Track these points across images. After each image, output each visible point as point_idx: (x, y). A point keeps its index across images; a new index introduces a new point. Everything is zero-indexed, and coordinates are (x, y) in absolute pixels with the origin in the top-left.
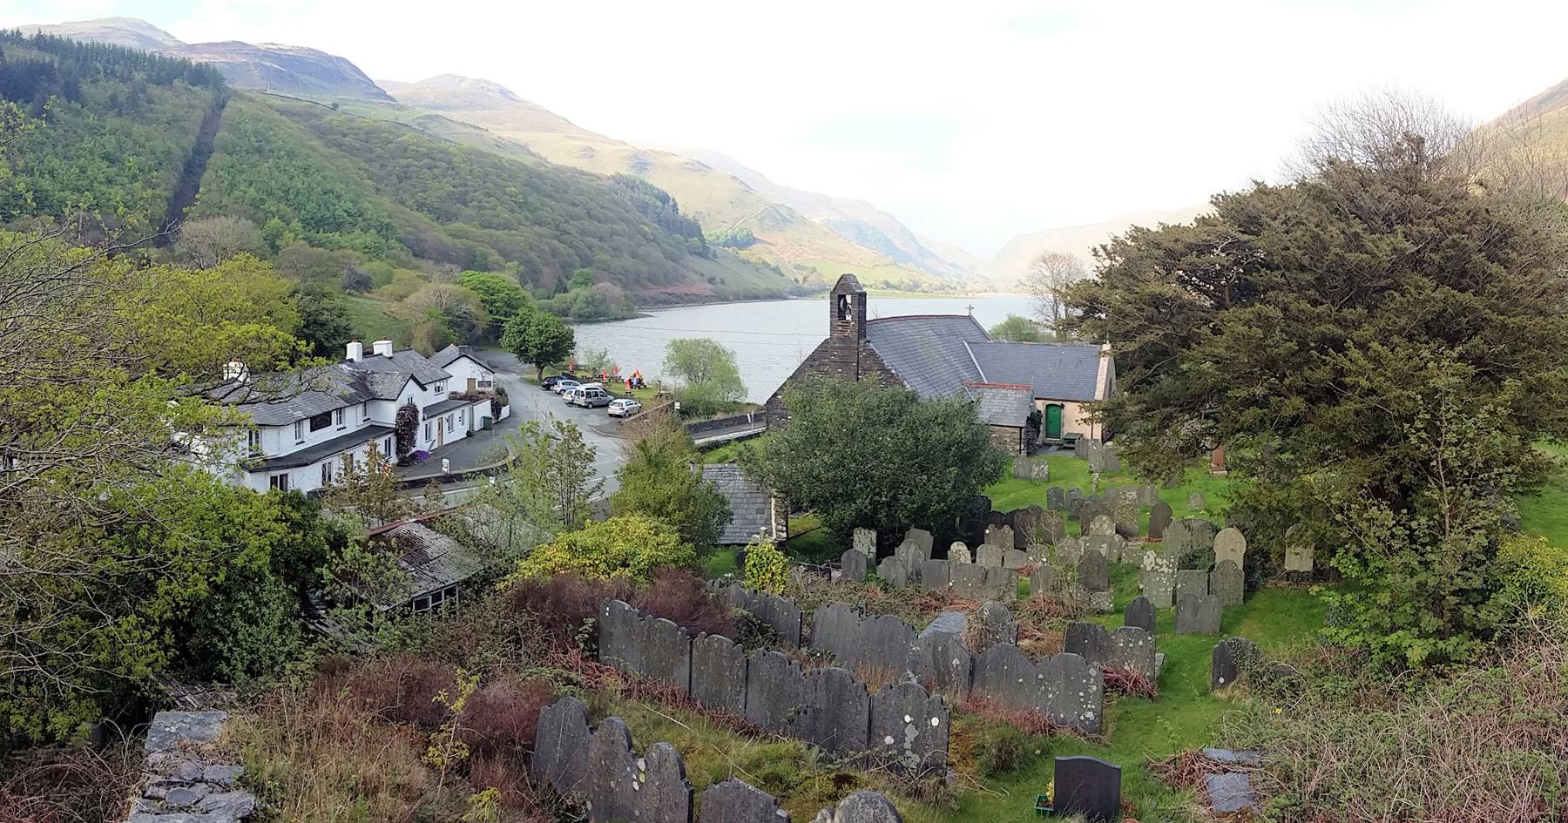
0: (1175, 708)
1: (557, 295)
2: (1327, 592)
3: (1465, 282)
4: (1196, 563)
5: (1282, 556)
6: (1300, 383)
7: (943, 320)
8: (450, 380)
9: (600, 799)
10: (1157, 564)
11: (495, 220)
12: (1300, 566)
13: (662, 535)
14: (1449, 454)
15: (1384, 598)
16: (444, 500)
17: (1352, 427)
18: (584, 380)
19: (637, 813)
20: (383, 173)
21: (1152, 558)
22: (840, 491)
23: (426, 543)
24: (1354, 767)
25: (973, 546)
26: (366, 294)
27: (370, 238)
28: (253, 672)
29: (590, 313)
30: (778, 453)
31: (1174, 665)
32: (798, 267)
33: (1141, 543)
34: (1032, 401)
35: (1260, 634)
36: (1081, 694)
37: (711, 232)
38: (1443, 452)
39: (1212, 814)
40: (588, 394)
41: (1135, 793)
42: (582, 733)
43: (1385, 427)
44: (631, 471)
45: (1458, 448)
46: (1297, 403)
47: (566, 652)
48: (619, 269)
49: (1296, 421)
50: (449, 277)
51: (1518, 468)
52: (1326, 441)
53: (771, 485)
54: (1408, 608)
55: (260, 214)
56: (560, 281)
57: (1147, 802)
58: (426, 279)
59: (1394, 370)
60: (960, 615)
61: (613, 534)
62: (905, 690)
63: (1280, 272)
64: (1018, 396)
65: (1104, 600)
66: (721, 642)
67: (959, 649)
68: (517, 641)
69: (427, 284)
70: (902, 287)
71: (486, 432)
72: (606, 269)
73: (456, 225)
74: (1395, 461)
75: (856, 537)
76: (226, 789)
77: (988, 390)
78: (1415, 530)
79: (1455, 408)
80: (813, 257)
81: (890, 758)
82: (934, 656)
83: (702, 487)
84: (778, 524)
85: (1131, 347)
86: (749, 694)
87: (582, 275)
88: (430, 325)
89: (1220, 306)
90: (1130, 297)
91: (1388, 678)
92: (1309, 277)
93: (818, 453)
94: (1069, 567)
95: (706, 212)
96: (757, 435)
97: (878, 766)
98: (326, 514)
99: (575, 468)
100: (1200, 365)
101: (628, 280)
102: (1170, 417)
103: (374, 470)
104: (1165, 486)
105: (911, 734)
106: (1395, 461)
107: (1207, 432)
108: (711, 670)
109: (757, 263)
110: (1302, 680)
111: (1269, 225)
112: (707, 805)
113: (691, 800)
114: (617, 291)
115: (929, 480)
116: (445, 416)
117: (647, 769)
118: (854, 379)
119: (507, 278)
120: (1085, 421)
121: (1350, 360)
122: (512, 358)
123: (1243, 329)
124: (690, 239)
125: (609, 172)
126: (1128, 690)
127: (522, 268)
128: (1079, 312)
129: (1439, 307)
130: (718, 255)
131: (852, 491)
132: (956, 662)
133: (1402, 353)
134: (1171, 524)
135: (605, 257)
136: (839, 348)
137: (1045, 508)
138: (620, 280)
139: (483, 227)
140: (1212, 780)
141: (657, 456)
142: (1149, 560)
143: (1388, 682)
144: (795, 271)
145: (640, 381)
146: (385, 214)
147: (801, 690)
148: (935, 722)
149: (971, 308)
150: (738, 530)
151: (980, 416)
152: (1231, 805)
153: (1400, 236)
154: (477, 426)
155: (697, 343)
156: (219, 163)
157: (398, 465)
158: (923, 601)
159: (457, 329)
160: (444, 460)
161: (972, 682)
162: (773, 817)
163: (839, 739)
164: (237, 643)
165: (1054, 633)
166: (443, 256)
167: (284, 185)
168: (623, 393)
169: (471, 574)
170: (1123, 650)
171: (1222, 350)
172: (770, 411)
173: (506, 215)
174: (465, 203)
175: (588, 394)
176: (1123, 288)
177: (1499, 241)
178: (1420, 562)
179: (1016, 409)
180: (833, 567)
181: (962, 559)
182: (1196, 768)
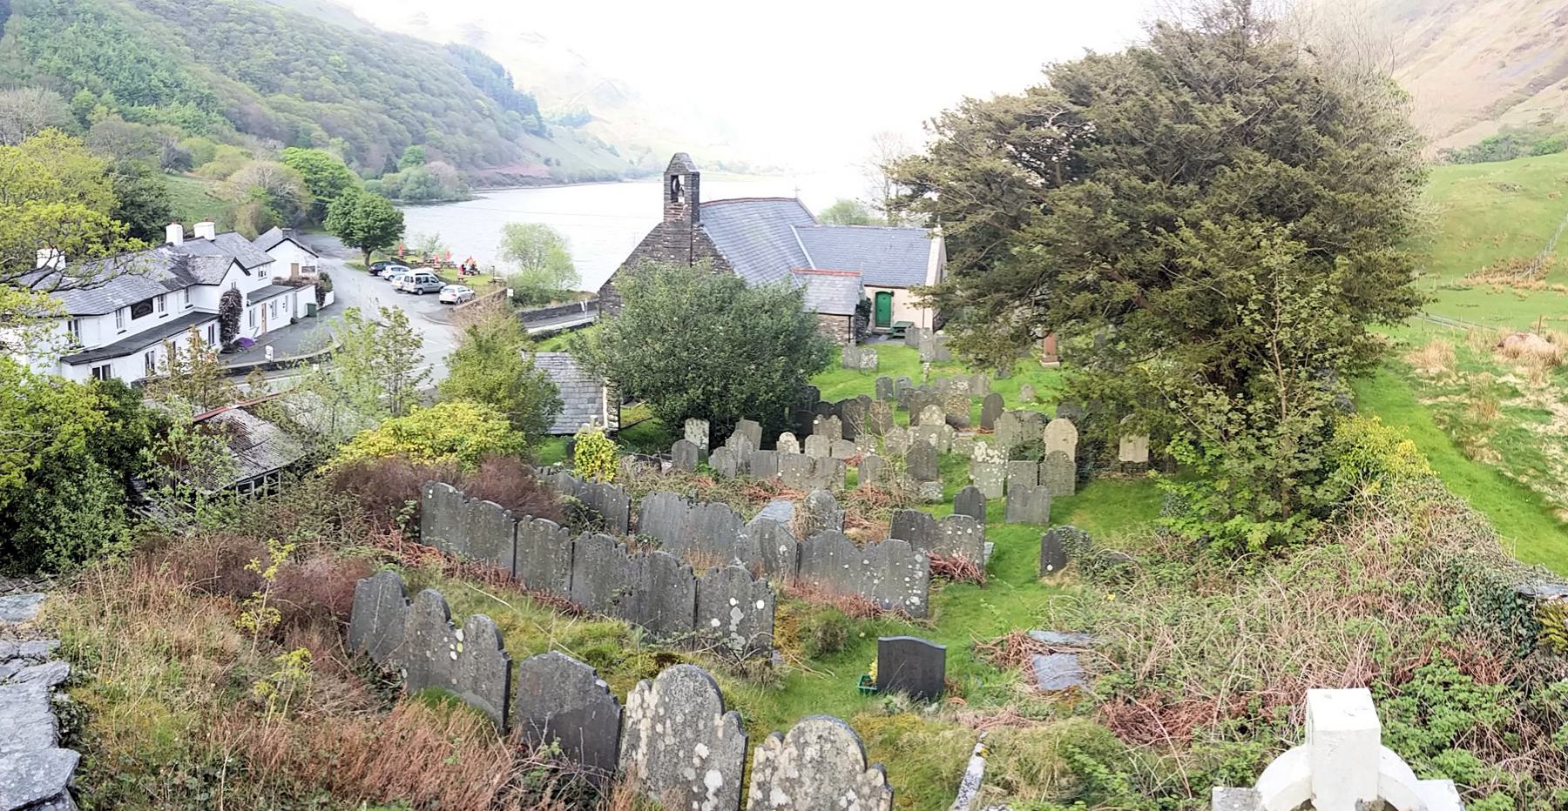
0: (1004, 594)
1: (385, 175)
2: (1162, 481)
3: (1296, 156)
4: (1026, 454)
5: (1117, 447)
6: (1132, 266)
7: (770, 203)
8: (273, 264)
9: (415, 669)
10: (988, 455)
11: (318, 91)
12: (1135, 458)
13: (491, 421)
14: (1284, 335)
15: (1223, 485)
16: (267, 388)
17: (1185, 312)
18: (415, 265)
19: (454, 681)
20: (201, 38)
21: (983, 448)
22: (671, 381)
23: (249, 430)
24: (1190, 647)
25: (801, 436)
26: (186, 173)
27: (190, 111)
28: (78, 558)
29: (422, 194)
30: (610, 340)
31: (1004, 553)
32: (633, 148)
33: (973, 434)
34: (861, 288)
35: (1092, 524)
37: (549, 109)
38: (1277, 333)
39: (1038, 692)
41: (959, 674)
43: (1220, 310)
44: (460, 356)
45: (1292, 329)
46: (1129, 288)
47: (387, 533)
48: (453, 147)
49: (1129, 306)
51: (1351, 349)
52: (1159, 327)
54: (1246, 494)
55: (67, 86)
56: (389, 159)
57: (973, 682)
58: (249, 156)
59: (1227, 250)
60: (789, 503)
61: (440, 420)
62: (730, 574)
63: (1110, 147)
65: (933, 490)
66: (546, 526)
68: (337, 522)
69: (251, 161)
71: (310, 319)
72: (439, 147)
74: (1230, 346)
75: (687, 428)
76: (42, 660)
77: (816, 276)
78: (1251, 414)
79: (1290, 288)
81: (717, 640)
82: (761, 543)
83: (534, 375)
85: (961, 228)
87: (412, 153)
88: (253, 206)
89: (1052, 184)
90: (960, 174)
91: (1227, 563)
92: (1139, 150)
93: (650, 341)
94: (897, 457)
97: (704, 647)
98: (149, 403)
99: (401, 355)
100: (1030, 251)
101: (464, 160)
102: (1001, 303)
103: (196, 357)
104: (1000, 375)
105: (737, 616)
106: (1230, 346)
107: (1038, 320)
110: (1136, 567)
111: (1098, 95)
112: (524, 676)
113: (509, 671)
114: (451, 171)
115: (757, 369)
116: (269, 302)
118: (687, 264)
119: (331, 155)
120: (915, 305)
121: (1182, 240)
122: (335, 242)
123: (1072, 208)
124: (527, 117)
125: (444, 40)
126: (956, 576)
127: (347, 144)
128: (907, 191)
129: (1271, 182)
131: (684, 381)
132: (783, 548)
133: (1233, 231)
135: (439, 134)
136: (672, 233)
137: (874, 398)
138: (454, 159)
139: (306, 99)
140: (1038, 660)
141: (487, 341)
142: (980, 451)
143: (1228, 566)
145: (473, 267)
146: (206, 84)
147: (627, 572)
148: (760, 604)
150: (569, 420)
152: (1057, 684)
153: (1229, 107)
154: (302, 313)
155: (533, 228)
156: (18, 26)
157: (222, 352)
158: (752, 491)
159: (281, 211)
160: (268, 347)
162: (592, 687)
163: (663, 622)
164: (59, 529)
165: (880, 523)
166: (266, 131)
167: (93, 52)
168: (456, 279)
169: (293, 460)
170: (951, 538)
171: (1052, 231)
172: (604, 298)
173: (330, 86)
174: (287, 73)
175: (418, 279)
176: (953, 164)
177: (1328, 112)
178: (1257, 448)
180: (663, 457)
181: (791, 450)
182: (1022, 649)
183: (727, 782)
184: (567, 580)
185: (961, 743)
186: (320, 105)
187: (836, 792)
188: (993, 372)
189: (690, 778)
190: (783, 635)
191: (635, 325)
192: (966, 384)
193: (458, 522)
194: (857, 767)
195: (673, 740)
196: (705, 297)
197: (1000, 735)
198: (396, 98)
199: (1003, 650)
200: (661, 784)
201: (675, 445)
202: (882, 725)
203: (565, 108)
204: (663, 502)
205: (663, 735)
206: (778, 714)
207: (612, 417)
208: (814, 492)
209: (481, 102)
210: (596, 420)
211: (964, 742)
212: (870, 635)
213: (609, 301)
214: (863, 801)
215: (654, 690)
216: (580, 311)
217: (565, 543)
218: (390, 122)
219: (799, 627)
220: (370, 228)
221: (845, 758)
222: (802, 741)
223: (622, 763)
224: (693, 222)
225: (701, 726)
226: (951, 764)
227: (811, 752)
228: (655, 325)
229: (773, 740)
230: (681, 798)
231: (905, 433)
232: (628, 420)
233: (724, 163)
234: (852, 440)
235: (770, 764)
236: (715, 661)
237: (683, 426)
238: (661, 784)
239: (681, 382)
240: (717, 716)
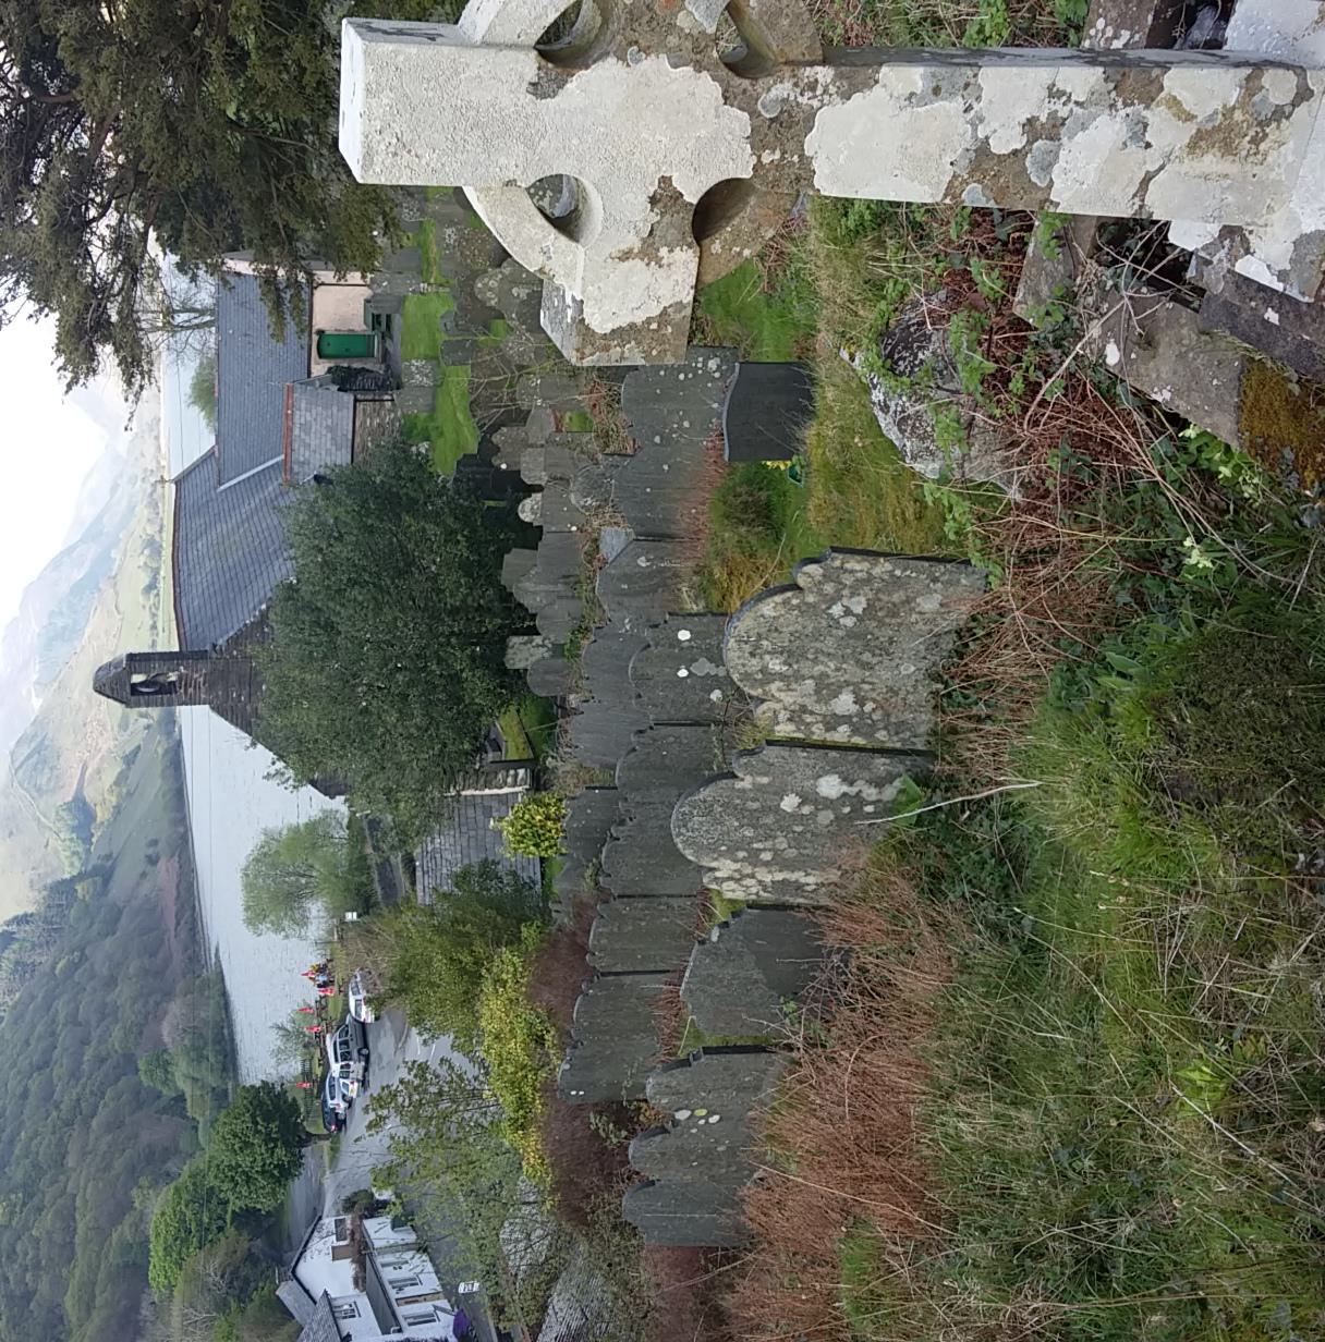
7: (183, 521)
8: (333, 1295)
23: (564, 1329)
29: (218, 1053)
36: (682, 377)
40: (346, 1056)
42: (666, 1190)
50: (160, 1310)
56: (164, 1111)
64: (303, 405)
66: (599, 936)
70: (155, 565)
73: (69, 1304)
82: (637, 594)
84: (505, 783)
95: (29, 873)
99: (440, 1093)
101: (157, 988)
108: (642, 946)
109: (119, 795)
114: (175, 1009)
116: (393, 1294)
117: (687, 1108)
119: (157, 1207)
122: (298, 1188)
127: (143, 1181)
130: (107, 852)
132: (642, 562)
135: (117, 1032)
136: (226, 690)
138: (157, 1004)
139: (71, 1258)
144: (131, 729)
145: (321, 970)
148: (684, 635)
155: (249, 887)
159: (252, 1284)
161: (671, 537)
173: (48, 1218)
174: (28, 1296)
179: (325, 408)
184: (675, 902)
186: (79, 1231)
189: (832, 817)
192: (449, 231)
193: (613, 1053)
194: (795, 602)
198: (62, 1106)
203: (62, 836)
204: (587, 736)
207: (509, 780)
208: (573, 501)
209: (59, 966)
214: (846, 592)
215: (714, 864)
217: (620, 907)
218: (103, 1114)
220: (268, 1139)
221: (782, 620)
222: (760, 676)
225: (756, 805)
227: (776, 665)
233: (145, 580)
235: (797, 715)
240: (739, 785)
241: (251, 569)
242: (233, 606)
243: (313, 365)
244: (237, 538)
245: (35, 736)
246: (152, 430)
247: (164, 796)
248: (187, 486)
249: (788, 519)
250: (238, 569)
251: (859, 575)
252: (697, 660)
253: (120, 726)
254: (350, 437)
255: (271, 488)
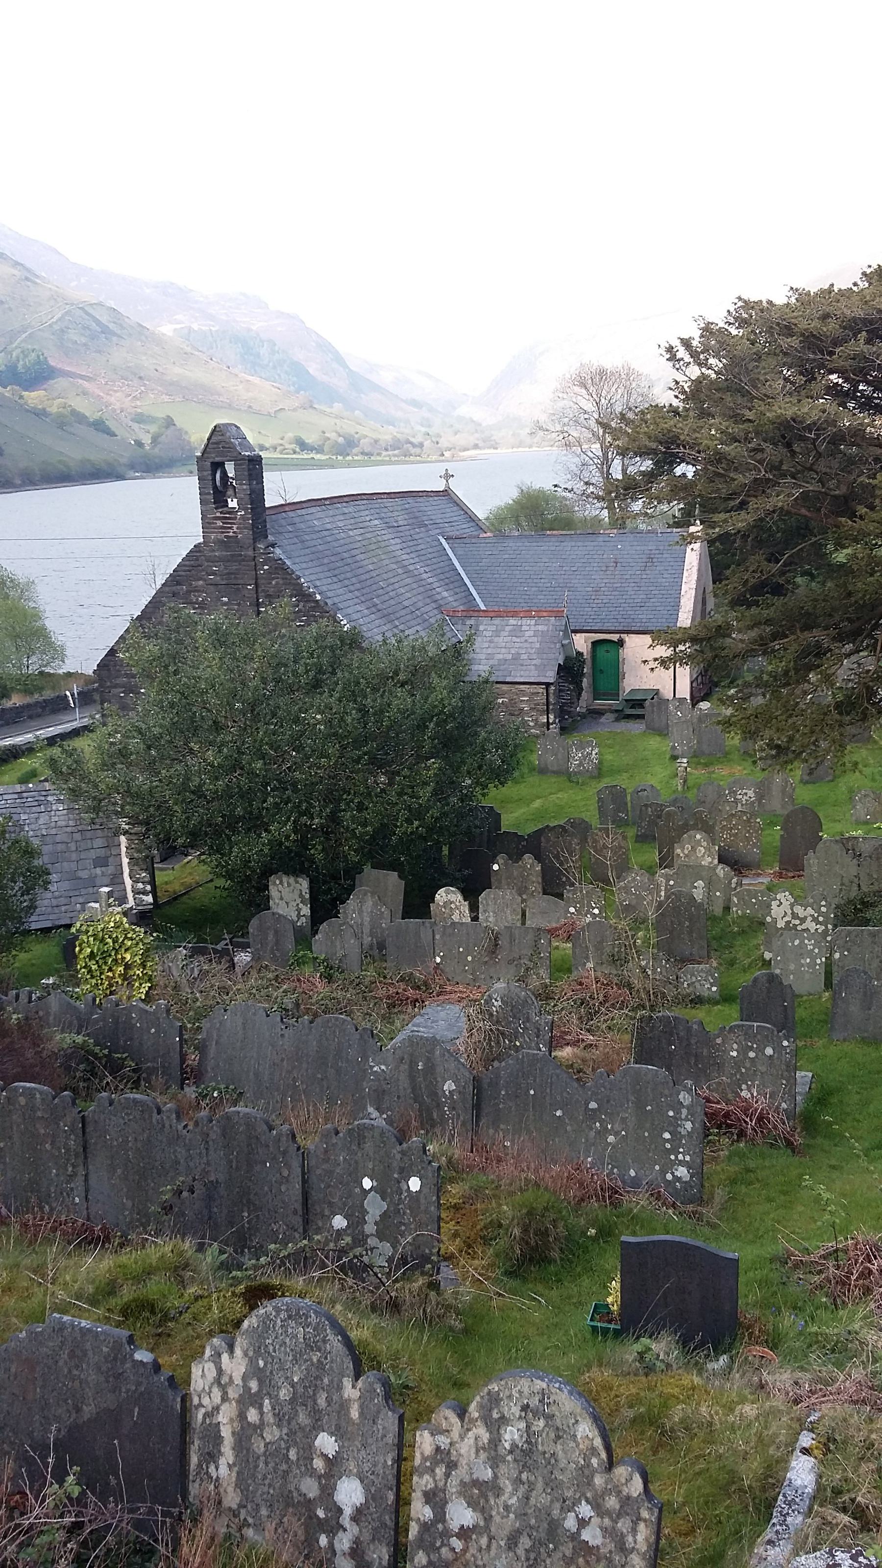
0: (833, 1167)
10: (795, 916)
21: (786, 904)
22: (239, 811)
25: (471, 894)
31: (830, 1093)
32: (140, 419)
33: (766, 880)
36: (667, 1136)
41: (764, 1305)
53: (116, 813)
57: (788, 1321)
60: (457, 1008)
62: (359, 1135)
64: (540, 628)
67: (452, 1065)
70: (326, 448)
75: (273, 891)
77: (486, 621)
80: (166, 398)
81: (343, 1252)
82: (412, 1077)
84: (136, 881)
85: (741, 521)
86: (93, 1181)
90: (736, 429)
93: (196, 747)
94: (639, 922)
96: (86, 729)
97: (323, 1266)
102: (819, 652)
104: (812, 777)
105: (375, 1208)
115: (391, 784)
126: (749, 1131)
128: (647, 465)
132: (449, 1086)
134: (821, 845)
136: (220, 559)
137: (595, 822)
144: (135, 426)
147: (181, 1152)
148: (415, 1184)
149: (448, 476)
150: (63, 901)
151: (475, 667)
158: (392, 990)
170: (738, 1063)
179: (540, 652)
181: (456, 917)
183: (372, 1496)
184: (78, 1183)
185: (773, 1429)
187: (558, 1505)
188: (798, 771)
189: (311, 1495)
190: (456, 1235)
191: (167, 722)
192: (751, 793)
194: (594, 1461)
195: (277, 1433)
196: (286, 666)
197: (845, 1420)
199: (838, 1267)
200: (264, 1512)
201: (254, 922)
202: (634, 1391)
205: (259, 1427)
206: (455, 1371)
207: (140, 885)
210: (110, 894)
211: (780, 1427)
212: (606, 1233)
213: (116, 686)
214: (607, 1521)
215: (238, 1352)
216: (66, 707)
217: (69, 1119)
219: (483, 1220)
221: (572, 1444)
222: (495, 1415)
223: (194, 1489)
224: (255, 540)
225: (322, 1401)
226: (756, 1464)
227: (511, 1434)
228: (203, 718)
229: (447, 1416)
230: (296, 1527)
231: (652, 881)
232: (170, 888)
233: (311, 439)
234: (560, 896)
236: (343, 1289)
237: (267, 887)
238: (264, 1512)
239: (256, 812)
240: (347, 1383)
241: (354, 580)
242: (315, 563)
243: (583, 634)
244: (385, 562)
245: (122, 327)
246: (484, 441)
247: (60, 462)
248: (441, 501)
249: (530, 1286)
250: (353, 566)
251: (630, 1539)
252: (383, 1199)
253: (141, 414)
254: (508, 679)
255: (445, 594)
